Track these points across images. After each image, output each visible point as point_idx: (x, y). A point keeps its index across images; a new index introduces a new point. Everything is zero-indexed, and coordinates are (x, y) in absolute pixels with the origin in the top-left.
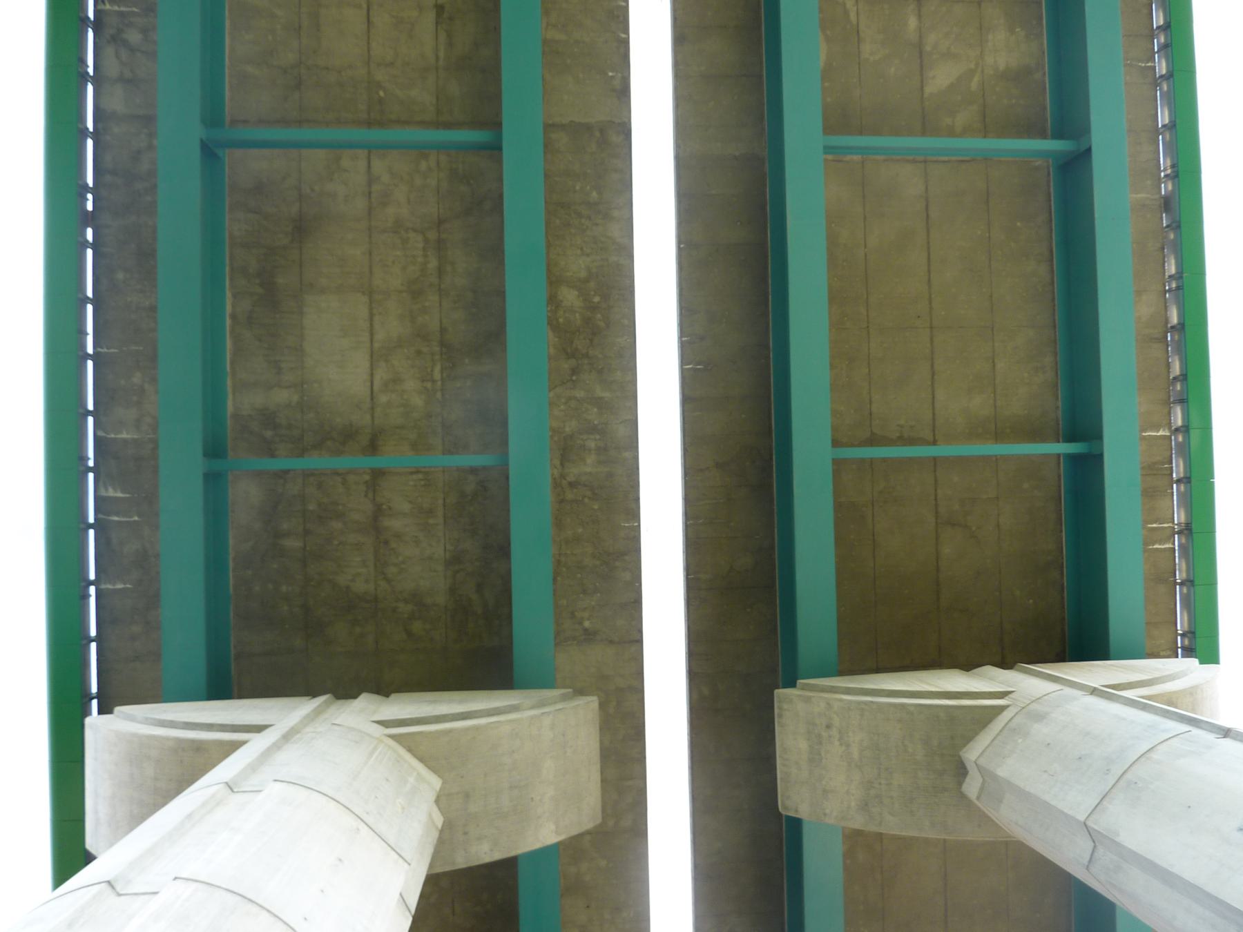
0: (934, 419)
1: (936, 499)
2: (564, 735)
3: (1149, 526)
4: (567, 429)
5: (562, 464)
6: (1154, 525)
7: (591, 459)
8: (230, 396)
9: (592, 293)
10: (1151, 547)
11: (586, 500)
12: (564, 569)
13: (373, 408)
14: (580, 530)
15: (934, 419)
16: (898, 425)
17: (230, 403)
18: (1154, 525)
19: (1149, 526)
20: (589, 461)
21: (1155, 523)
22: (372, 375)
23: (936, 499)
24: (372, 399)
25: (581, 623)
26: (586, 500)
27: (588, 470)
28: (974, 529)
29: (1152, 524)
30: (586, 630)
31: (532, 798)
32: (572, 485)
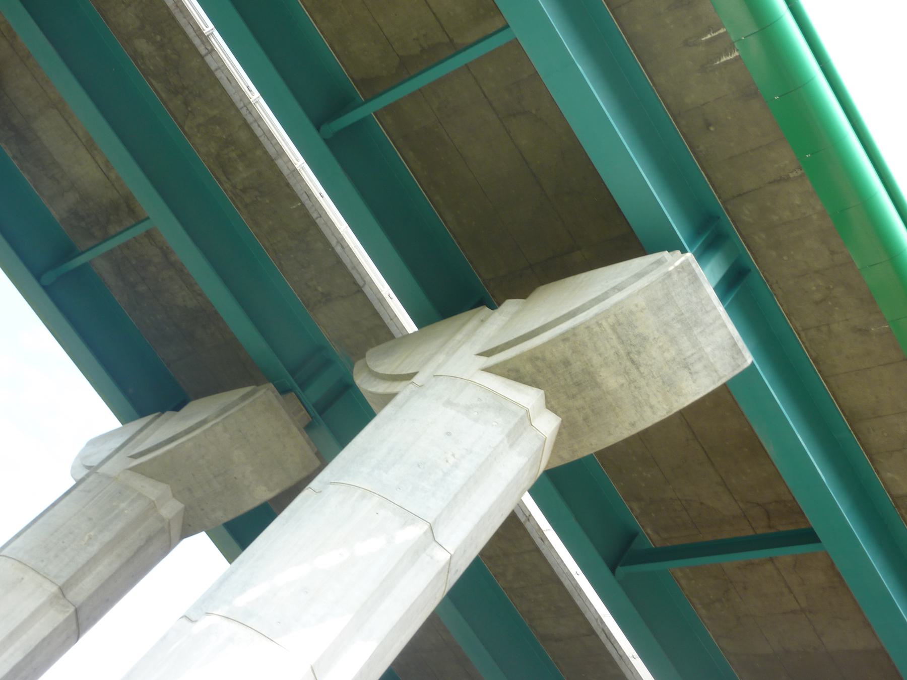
0: (438, 20)
1: (485, 96)
2: (240, 431)
3: (703, 39)
4: (213, 151)
5: (228, 179)
6: (709, 36)
7: (241, 166)
8: (51, 209)
9: (153, 35)
10: (718, 63)
11: (259, 199)
12: (281, 255)
13: (113, 185)
14: (270, 222)
15: (438, 20)
16: (414, 39)
17: (54, 213)
18: (709, 36)
19: (703, 39)
20: (241, 169)
21: (708, 32)
22: (97, 163)
23: (485, 96)
24: (108, 178)
25: (316, 290)
26: (259, 199)
27: (245, 175)
28: (534, 112)
29: (706, 35)
30: (322, 293)
31: (235, 478)
32: (244, 190)
